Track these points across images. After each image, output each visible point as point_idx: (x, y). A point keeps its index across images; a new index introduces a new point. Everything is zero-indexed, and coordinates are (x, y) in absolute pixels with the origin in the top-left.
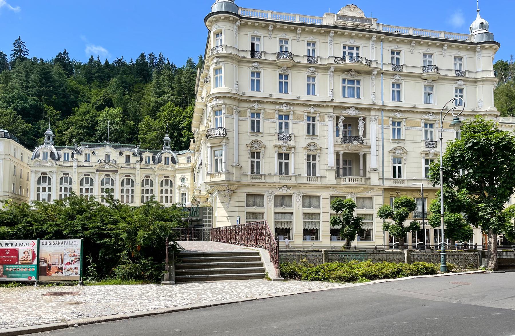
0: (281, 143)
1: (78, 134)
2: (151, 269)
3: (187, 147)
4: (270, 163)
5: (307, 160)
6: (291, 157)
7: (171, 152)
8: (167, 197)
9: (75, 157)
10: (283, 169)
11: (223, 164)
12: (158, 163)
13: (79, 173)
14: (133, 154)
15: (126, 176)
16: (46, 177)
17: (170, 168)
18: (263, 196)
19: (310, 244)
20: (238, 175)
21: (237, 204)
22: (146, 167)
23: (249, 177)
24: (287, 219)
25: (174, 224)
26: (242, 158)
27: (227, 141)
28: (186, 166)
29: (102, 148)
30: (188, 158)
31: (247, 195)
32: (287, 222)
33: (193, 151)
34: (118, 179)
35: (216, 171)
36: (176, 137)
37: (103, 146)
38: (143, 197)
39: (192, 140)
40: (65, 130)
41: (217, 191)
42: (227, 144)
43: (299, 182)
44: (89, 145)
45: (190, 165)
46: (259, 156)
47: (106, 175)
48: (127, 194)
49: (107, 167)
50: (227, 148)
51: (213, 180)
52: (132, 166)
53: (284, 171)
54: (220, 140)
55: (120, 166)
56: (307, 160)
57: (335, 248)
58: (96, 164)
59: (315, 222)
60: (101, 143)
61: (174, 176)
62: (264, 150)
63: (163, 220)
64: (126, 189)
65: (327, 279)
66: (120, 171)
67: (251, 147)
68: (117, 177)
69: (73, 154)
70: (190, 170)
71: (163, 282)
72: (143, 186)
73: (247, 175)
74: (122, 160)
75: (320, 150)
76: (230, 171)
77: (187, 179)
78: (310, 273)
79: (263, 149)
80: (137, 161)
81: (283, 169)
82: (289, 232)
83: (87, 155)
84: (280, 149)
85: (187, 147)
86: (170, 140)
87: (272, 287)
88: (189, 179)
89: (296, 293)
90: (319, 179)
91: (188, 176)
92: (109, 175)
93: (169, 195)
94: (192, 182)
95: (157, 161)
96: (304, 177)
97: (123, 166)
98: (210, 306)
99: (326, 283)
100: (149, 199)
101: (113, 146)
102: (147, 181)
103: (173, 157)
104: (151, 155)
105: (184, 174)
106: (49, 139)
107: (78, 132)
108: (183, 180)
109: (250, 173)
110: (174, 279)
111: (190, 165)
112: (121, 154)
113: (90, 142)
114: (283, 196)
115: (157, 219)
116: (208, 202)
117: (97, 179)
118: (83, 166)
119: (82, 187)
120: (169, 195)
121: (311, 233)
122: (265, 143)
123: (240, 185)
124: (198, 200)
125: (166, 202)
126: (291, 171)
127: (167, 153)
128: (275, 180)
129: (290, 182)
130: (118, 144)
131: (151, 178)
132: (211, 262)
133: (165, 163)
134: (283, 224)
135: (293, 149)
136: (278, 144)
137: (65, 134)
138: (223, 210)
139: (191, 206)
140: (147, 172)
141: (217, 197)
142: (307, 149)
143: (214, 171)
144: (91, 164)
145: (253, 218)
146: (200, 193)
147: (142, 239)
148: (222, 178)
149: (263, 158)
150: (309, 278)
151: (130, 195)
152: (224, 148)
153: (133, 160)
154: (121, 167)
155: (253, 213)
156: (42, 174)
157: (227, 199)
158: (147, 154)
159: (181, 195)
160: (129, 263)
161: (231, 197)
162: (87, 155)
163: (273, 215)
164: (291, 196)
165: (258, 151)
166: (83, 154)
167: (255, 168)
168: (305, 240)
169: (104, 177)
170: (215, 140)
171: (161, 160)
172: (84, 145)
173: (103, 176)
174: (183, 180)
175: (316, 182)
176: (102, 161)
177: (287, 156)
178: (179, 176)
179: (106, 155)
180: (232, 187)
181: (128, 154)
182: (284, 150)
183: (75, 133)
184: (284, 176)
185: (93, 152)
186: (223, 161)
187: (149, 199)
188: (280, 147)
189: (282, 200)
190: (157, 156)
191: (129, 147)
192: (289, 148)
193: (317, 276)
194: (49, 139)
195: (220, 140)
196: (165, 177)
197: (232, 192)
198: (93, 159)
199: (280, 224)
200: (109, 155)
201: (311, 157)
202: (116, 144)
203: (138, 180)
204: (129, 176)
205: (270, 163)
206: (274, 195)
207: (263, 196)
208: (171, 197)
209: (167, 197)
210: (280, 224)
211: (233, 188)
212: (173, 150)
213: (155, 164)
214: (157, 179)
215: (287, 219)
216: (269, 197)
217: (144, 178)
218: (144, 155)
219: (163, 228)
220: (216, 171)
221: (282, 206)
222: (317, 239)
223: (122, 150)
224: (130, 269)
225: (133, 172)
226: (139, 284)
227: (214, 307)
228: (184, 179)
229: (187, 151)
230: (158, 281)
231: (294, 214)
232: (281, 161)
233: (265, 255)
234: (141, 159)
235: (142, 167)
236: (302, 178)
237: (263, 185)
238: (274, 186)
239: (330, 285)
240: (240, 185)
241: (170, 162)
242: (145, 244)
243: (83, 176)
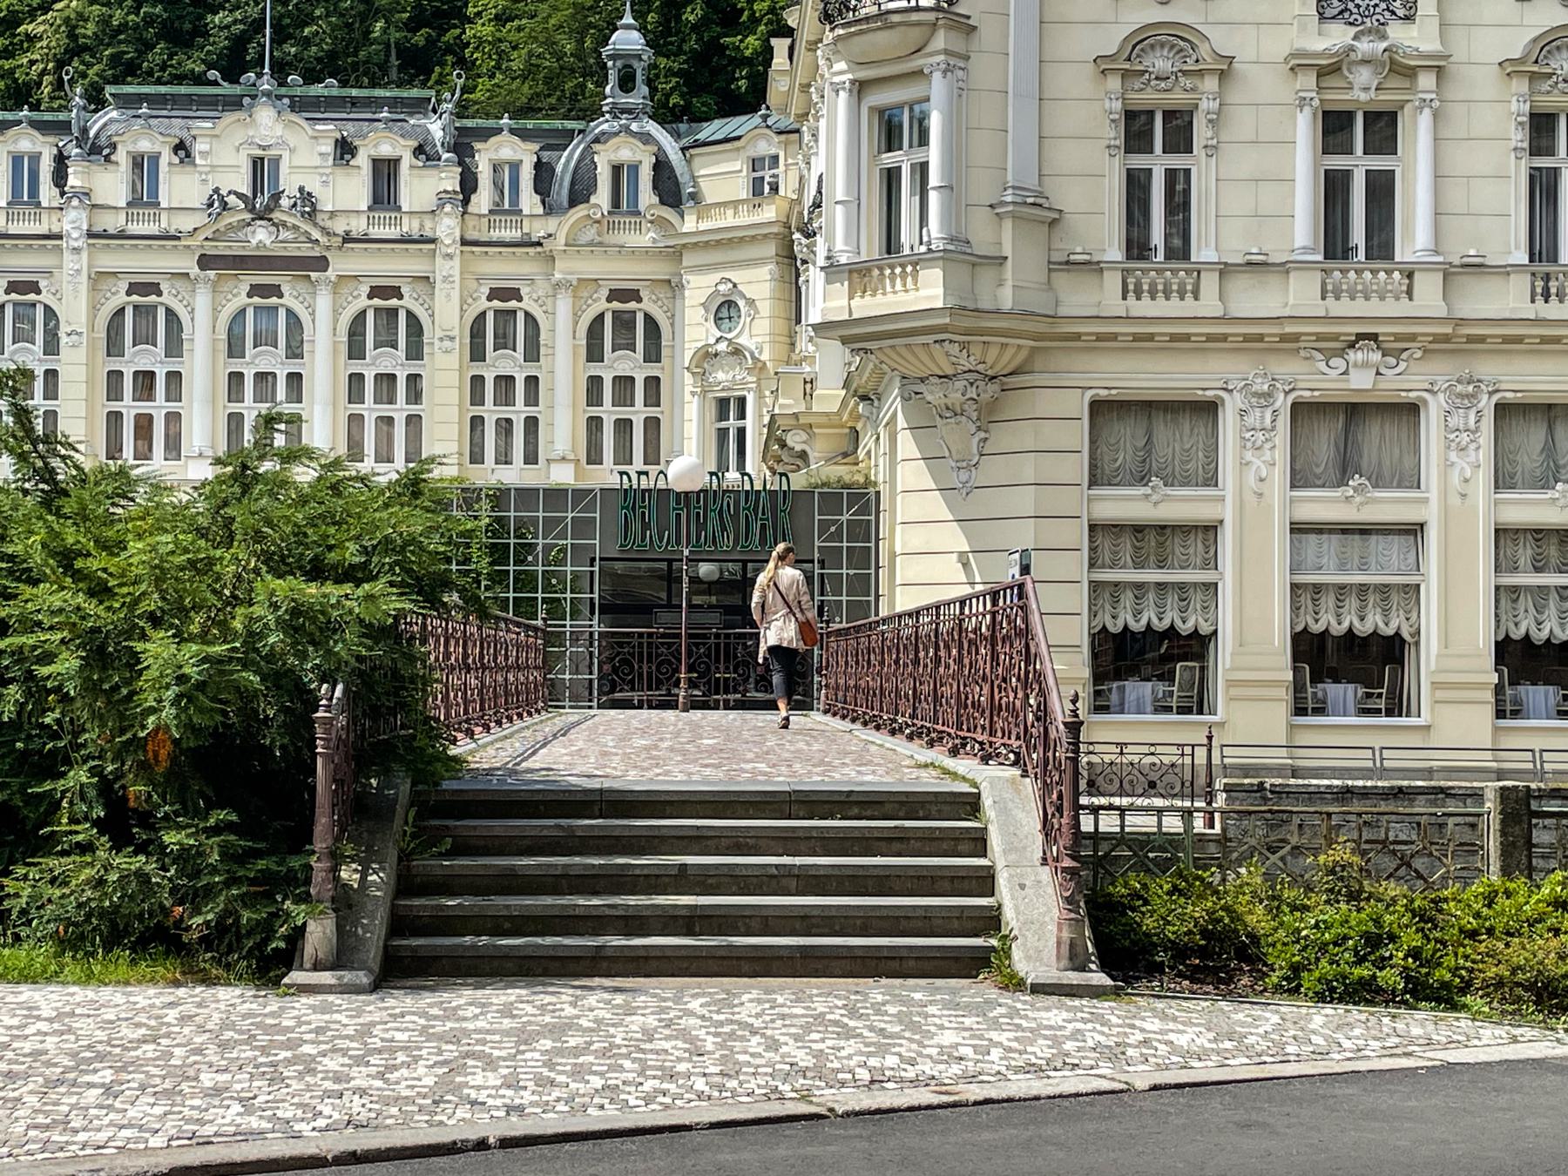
0: (1338, 36)
1: (110, 34)
2: (228, 884)
3: (752, 100)
4: (1259, 186)
5: (1535, 151)
6: (1417, 134)
7: (653, 127)
8: (624, 426)
9: (73, 181)
10: (1357, 220)
11: (934, 198)
12: (574, 202)
13: (99, 278)
14: (419, 151)
15: (375, 292)
16: (393, 312)
17: (647, 238)
18: (1208, 409)
19: (1347, 743)
20: (1035, 271)
21: (1028, 469)
22: (495, 235)
23: (1113, 281)
24: (1384, 565)
25: (370, 598)
26: (1066, 156)
27: (958, 45)
28: (745, 218)
29: (230, 118)
30: (755, 164)
31: (1097, 407)
32: (1384, 590)
33: (787, 122)
34: (324, 315)
35: (891, 243)
36: (695, 28)
37: (235, 104)
38: (477, 422)
39: (780, 45)
40: (32, 14)
41: (897, 382)
42: (957, 61)
43: (1466, 310)
44: (155, 101)
45: (769, 213)
46: (1179, 138)
47: (255, 290)
48: (385, 410)
49: (261, 237)
50: (960, 93)
51: (866, 306)
52: (409, 226)
53: (1358, 235)
54: (915, 35)
55: (340, 226)
56: (1535, 151)
57: (1384, 772)
58: (199, 219)
59: (1182, 586)
60: (226, 89)
61: (673, 287)
62: (1220, 95)
63: (317, 572)
64: (290, 375)
65: (1446, 998)
66: (340, 265)
67: (1126, 74)
68: (323, 302)
69: (61, 160)
70: (770, 249)
71: (296, 977)
72: (477, 354)
73: (1094, 267)
74: (348, 192)
75: (1222, 74)
76: (982, 242)
77: (751, 302)
78: (1323, 947)
79: (1210, 84)
80: (443, 198)
81: (1357, 220)
82: (1399, 661)
83: (143, 166)
84: (1330, 81)
85: (752, 100)
86: (647, 56)
87: (1032, 1035)
88: (765, 308)
89: (1141, 1084)
90: (1209, 282)
91: (758, 281)
92: (276, 291)
93: (638, 413)
94: (782, 325)
95: (561, 191)
96: (1505, 271)
97: (358, 226)
98: (482, 1145)
99: (1419, 1023)
100: (248, 437)
101: (300, 105)
102: (501, 324)
103: (662, 167)
104: (526, 154)
105: (734, 275)
106: (627, 83)
107: (105, 21)
108: (725, 309)
109: (1115, 253)
110: (373, 954)
111: (769, 213)
112: (345, 149)
113: (179, 79)
114: (1354, 412)
115: (279, 565)
116: (861, 454)
117: (204, 312)
118: (122, 235)
119: (115, 364)
120: (638, 413)
121: (1352, 662)
122: (1221, 40)
123: (1052, 337)
124: (796, 440)
125: (504, 458)
126: (1414, 236)
127: (625, 142)
128: (1299, 297)
129: (1403, 308)
130: (328, 88)
131: (527, 304)
132: (642, 852)
133: (616, 202)
134: (1352, 603)
135: (1426, 81)
136: (1319, 45)
137: (31, 39)
138: (937, 506)
139: (700, 482)
140: (503, 268)
141: (901, 422)
142: (1533, 77)
143: (872, 247)
144: (165, 223)
145: (1139, 565)
146: (808, 395)
147: (170, 694)
148: (927, 292)
149: (1212, 150)
150: (1308, 981)
151: (400, 410)
152: (938, 87)
153: (421, 188)
154: (348, 238)
155: (1138, 530)
156: (375, 292)
157: (959, 436)
158: (505, 149)
159: (712, 411)
160: (86, 848)
161: (987, 417)
162: (143, 166)
163: (1278, 543)
164: (1411, 411)
165: (1177, 98)
166: (121, 156)
167: (1157, 221)
168: (1516, 714)
169: (243, 299)
170: (882, 38)
171: (592, 187)
172: (126, 102)
173: (238, 296)
174: (725, 309)
175: (1188, 307)
176: (232, 200)
177: (1383, 129)
178: (699, 287)
179: (257, 163)
180: (993, 353)
181: (386, 150)
182: (1361, 89)
183: (91, 29)
184: (1358, 271)
185: (180, 147)
186: (934, 179)
187: (248, 437)
188: (1330, 69)
189: (1348, 433)
190: (565, 162)
191: (394, 104)
192: (1399, 68)
193: (1363, 972)
194: (627, 83)
195: (915, 35)
196: (614, 295)
197: (993, 388)
198: (181, 190)
199: (1328, 601)
200: (276, 161)
201: (1357, 129)
202: (317, 89)
203: (446, 315)
204: (515, 294)
205: (1259, 186)
206: (1283, 403)
207: (1208, 409)
208: (532, 424)
209: (624, 426)
210: (1328, 601)
211: (1000, 358)
212: (666, 115)
213: (550, 210)
214: (564, 305)
215: (1384, 565)
216: (1250, 420)
217: (483, 304)
218: (485, 157)
219: (306, 625)
220: (891, 243)
221: (1342, 482)
222: (1396, 707)
223: (349, 130)
224: (101, 882)
225: (416, 266)
226: (153, 981)
227: (499, 1154)
228: (730, 304)
229: (756, 119)
230: (270, 965)
231: (1433, 535)
232: (1338, 162)
233: (1011, 806)
234: (468, 185)
235: (472, 235)
236: (1491, 284)
237: (1211, 338)
238: (1284, 338)
239: (1440, 1036)
240: (1052, 337)
241: (647, 196)
242: (189, 727)
243: (119, 297)
